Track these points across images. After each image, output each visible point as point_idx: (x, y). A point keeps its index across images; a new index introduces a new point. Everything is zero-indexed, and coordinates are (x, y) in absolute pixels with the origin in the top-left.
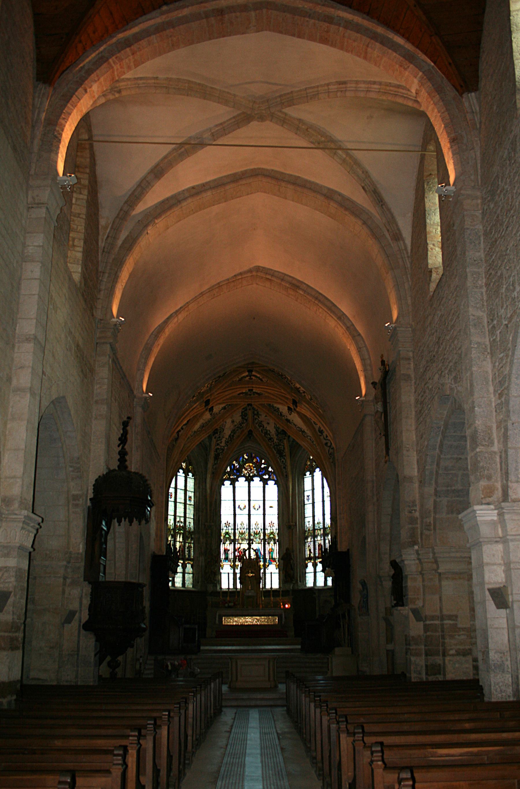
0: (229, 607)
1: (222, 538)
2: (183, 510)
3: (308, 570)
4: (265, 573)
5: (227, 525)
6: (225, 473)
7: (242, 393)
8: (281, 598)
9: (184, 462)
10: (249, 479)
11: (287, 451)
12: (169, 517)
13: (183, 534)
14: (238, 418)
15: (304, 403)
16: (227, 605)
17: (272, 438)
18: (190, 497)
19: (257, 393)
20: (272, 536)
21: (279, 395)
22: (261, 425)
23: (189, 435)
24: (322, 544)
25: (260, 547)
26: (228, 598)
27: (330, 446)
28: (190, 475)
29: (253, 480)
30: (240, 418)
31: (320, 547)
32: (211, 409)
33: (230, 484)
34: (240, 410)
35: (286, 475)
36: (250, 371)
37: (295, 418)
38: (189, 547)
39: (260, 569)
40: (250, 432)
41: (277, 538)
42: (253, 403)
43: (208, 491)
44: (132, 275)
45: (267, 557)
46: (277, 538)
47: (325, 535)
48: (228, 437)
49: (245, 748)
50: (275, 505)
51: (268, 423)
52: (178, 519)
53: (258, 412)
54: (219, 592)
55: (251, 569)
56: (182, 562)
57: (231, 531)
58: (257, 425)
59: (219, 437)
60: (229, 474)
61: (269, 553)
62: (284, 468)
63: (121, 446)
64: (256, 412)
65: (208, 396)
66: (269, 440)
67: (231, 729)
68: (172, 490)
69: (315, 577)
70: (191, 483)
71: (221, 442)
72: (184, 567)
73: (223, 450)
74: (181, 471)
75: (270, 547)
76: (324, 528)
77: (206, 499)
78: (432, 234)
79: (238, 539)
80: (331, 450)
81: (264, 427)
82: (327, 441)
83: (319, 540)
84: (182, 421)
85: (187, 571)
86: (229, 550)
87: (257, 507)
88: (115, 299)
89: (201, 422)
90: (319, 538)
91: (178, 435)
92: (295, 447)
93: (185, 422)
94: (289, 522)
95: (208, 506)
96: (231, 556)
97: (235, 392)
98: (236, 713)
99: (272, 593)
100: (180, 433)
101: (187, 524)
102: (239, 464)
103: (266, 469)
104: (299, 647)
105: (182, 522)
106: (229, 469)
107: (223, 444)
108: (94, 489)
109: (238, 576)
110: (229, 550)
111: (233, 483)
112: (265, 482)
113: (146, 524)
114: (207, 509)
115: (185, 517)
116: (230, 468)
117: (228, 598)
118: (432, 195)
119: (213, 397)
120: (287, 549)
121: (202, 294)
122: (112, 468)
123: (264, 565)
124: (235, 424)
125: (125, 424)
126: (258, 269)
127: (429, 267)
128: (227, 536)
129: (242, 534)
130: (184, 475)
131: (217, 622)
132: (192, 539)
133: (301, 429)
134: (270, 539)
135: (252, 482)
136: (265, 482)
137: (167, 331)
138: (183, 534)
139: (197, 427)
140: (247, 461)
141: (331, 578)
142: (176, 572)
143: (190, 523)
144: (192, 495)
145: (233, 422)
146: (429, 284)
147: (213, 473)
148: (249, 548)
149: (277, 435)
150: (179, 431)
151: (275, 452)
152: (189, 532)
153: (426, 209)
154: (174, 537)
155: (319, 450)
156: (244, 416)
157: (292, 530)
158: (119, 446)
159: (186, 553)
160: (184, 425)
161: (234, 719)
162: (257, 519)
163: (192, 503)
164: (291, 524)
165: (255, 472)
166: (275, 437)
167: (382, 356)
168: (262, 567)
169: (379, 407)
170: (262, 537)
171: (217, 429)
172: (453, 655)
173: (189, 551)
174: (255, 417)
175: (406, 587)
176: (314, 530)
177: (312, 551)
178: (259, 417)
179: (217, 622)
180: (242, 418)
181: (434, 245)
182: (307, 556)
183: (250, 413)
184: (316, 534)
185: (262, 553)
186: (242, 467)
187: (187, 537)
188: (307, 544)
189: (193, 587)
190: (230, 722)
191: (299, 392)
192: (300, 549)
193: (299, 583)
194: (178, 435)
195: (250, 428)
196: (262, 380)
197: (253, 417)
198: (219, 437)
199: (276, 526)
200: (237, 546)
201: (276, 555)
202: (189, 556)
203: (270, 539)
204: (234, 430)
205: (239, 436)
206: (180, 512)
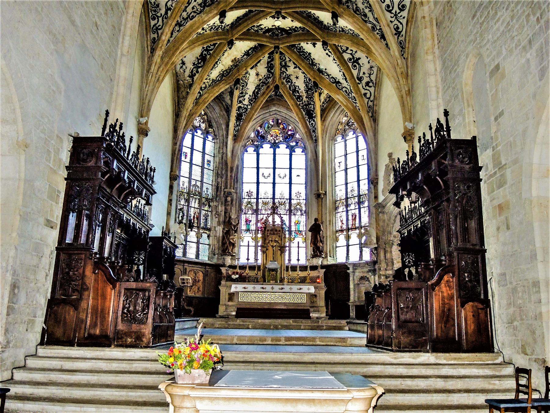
2: (199, 174)
5: (249, 194)
10: (275, 146)
14: (262, 69)
17: (301, 96)
22: (288, 78)
27: (369, 98)
28: (210, 138)
29: (279, 147)
31: (354, 216)
33: (254, 151)
35: (316, 140)
38: (206, 216)
41: (304, 209)
43: (229, 154)
45: (293, 228)
46: (304, 209)
48: (251, 94)
50: (303, 173)
51: (297, 78)
52: (193, 183)
53: (286, 63)
58: (284, 81)
62: (314, 131)
64: (283, 63)
66: (297, 99)
70: (210, 146)
73: (246, 109)
75: (297, 219)
76: (359, 196)
79: (261, 210)
81: (292, 82)
82: (366, 91)
85: (201, 241)
86: (250, 221)
87: (282, 176)
90: (352, 207)
94: (318, 190)
96: (253, 227)
101: (204, 189)
107: (246, 102)
110: (250, 221)
112: (292, 150)
114: (227, 175)
115: (202, 181)
124: (261, 78)
134: (296, 209)
135: (277, 149)
136: (292, 150)
138: (199, 199)
145: (257, 74)
147: (235, 136)
149: (307, 92)
151: (304, 113)
152: (207, 199)
157: (322, 199)
162: (282, 190)
164: (321, 192)
165: (281, 139)
166: (305, 95)
170: (287, 207)
174: (282, 69)
176: (347, 198)
177: (345, 222)
178: (287, 70)
179: (96, 248)
180: (268, 71)
184: (349, 202)
185: (288, 225)
187: (204, 204)
192: (330, 221)
195: (277, 83)
197: (281, 70)
199: (303, 196)
201: (302, 227)
203: (296, 209)
204: (258, 86)
205: (264, 93)
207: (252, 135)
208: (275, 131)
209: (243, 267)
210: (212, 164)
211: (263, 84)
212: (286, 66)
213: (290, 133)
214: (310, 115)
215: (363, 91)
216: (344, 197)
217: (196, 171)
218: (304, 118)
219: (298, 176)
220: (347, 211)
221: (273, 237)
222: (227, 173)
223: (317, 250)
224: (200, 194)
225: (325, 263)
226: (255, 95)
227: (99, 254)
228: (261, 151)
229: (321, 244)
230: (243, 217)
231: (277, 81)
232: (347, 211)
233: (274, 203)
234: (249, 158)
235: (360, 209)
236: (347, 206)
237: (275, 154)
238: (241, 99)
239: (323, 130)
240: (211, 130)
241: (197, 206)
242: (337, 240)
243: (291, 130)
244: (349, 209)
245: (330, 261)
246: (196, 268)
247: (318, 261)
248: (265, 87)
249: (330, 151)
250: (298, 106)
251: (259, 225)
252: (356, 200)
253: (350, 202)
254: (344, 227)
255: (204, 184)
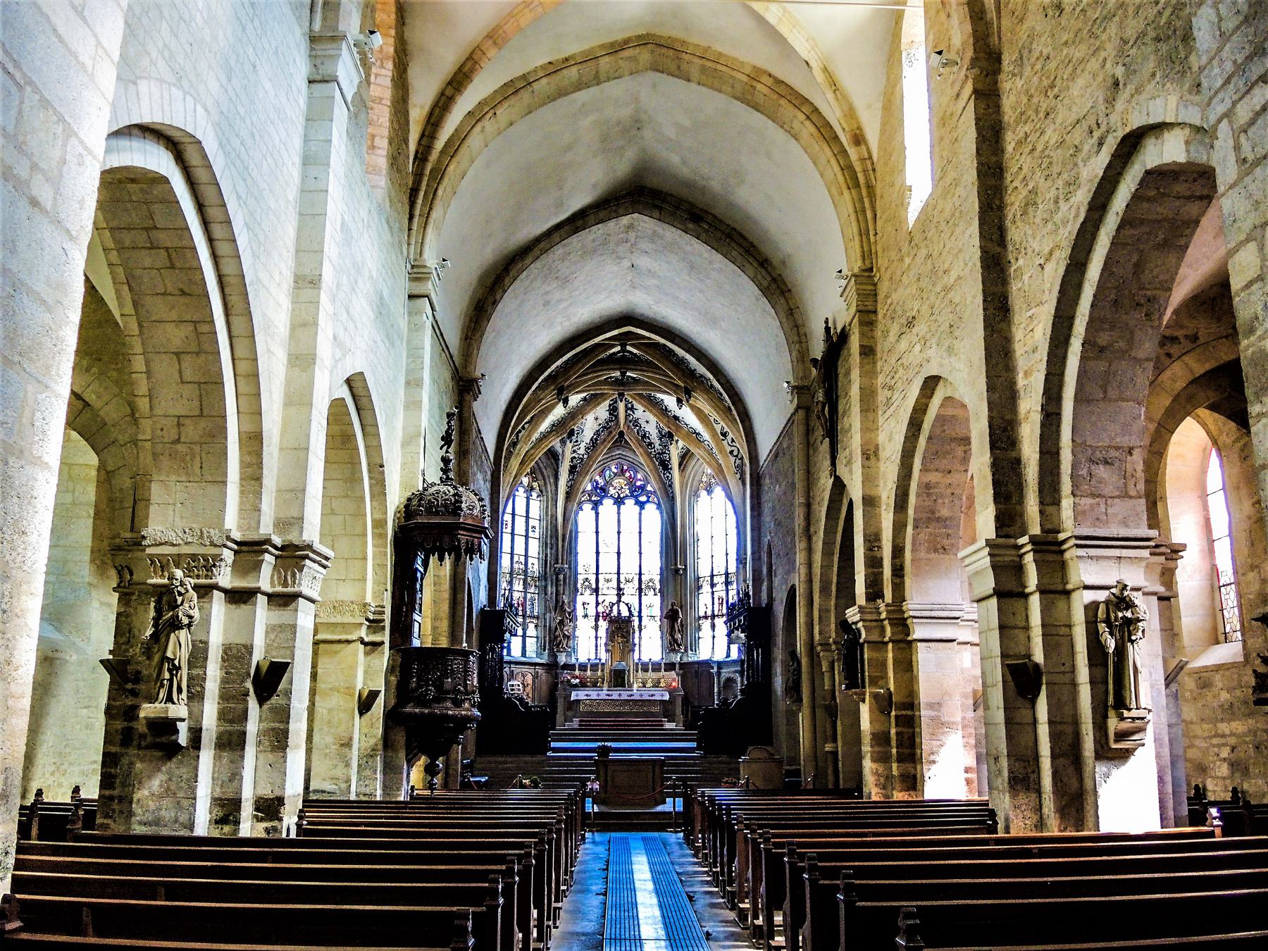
10: (619, 501)
22: (636, 423)
28: (534, 495)
41: (658, 587)
70: (535, 507)
76: (727, 574)
107: (582, 451)
134: (648, 587)
136: (641, 505)
166: (657, 443)
176: (712, 576)
207: (589, 488)
208: (619, 482)
209: (583, 667)
210: (537, 530)
213: (639, 483)
214: (665, 465)
215: (729, 448)
217: (519, 542)
218: (657, 470)
221: (621, 630)
222: (560, 544)
223: (672, 644)
225: (685, 660)
226: (594, 442)
227: (784, 933)
228: (601, 508)
230: (580, 599)
233: (619, 581)
234: (585, 517)
235: (727, 591)
236: (713, 585)
239: (682, 483)
240: (535, 485)
242: (699, 629)
245: (691, 658)
246: (525, 669)
247: (676, 658)
248: (606, 432)
249: (692, 509)
253: (716, 580)
254: (709, 613)
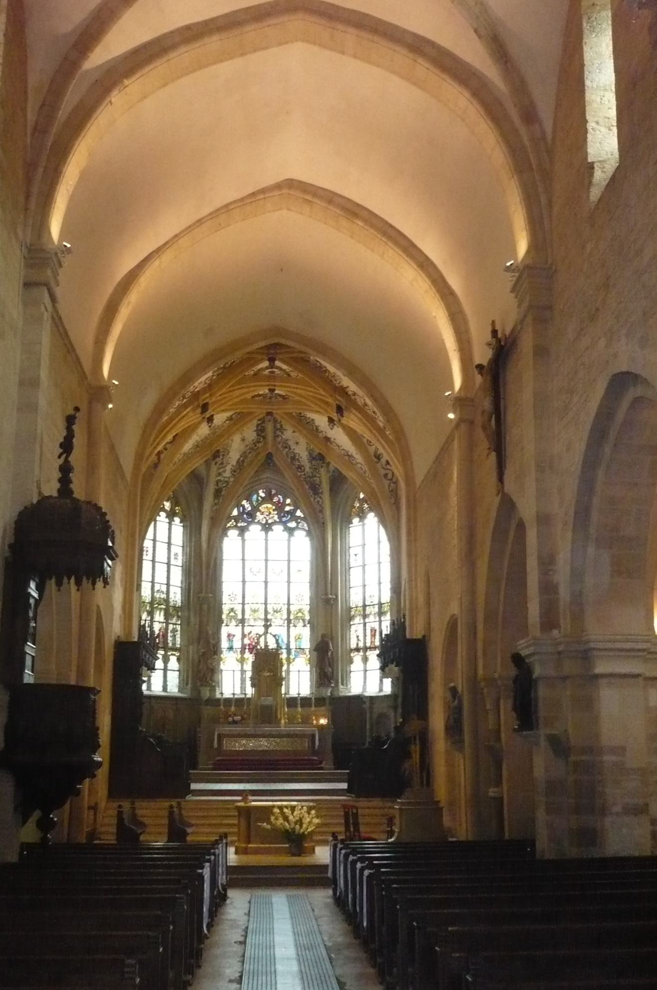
0: (235, 722)
1: (224, 617)
3: (353, 667)
4: (288, 671)
6: (230, 518)
7: (259, 395)
8: (313, 708)
9: (167, 501)
11: (325, 487)
12: (144, 584)
13: (165, 609)
14: (250, 433)
15: (354, 411)
16: (230, 719)
18: (176, 554)
19: (280, 395)
20: (300, 615)
21: (314, 397)
22: (286, 446)
23: (176, 459)
24: (377, 628)
25: (282, 632)
26: (233, 709)
27: (391, 479)
30: (255, 433)
32: (210, 420)
34: (255, 422)
36: (272, 360)
37: (339, 436)
38: (174, 631)
39: (282, 665)
40: (269, 456)
41: (307, 617)
42: (274, 412)
44: (84, 176)
45: (293, 646)
47: (381, 613)
48: (235, 463)
49: (273, 982)
52: (157, 587)
53: (281, 426)
54: (219, 700)
55: (268, 665)
56: (163, 652)
57: (238, 608)
59: (222, 463)
60: (237, 519)
61: (296, 640)
62: (321, 511)
63: (64, 456)
65: (206, 398)
67: (246, 937)
68: (148, 544)
69: (367, 679)
71: (224, 472)
72: (166, 660)
74: (163, 514)
76: (380, 605)
77: (201, 557)
78: (595, 105)
80: (392, 485)
82: (387, 472)
83: (372, 622)
84: (165, 436)
88: (56, 210)
89: (195, 439)
90: (371, 618)
91: (159, 459)
92: (337, 481)
93: (170, 437)
94: (326, 594)
95: (203, 573)
96: (237, 644)
97: (248, 392)
98: (250, 902)
99: (299, 702)
100: (162, 456)
102: (251, 504)
103: (292, 513)
104: (344, 786)
105: (163, 592)
106: (235, 513)
107: (227, 474)
108: (15, 529)
109: (249, 674)
111: (242, 531)
113: (105, 587)
114: (201, 573)
115: (168, 585)
116: (239, 510)
117: (233, 709)
118: (595, 40)
119: (214, 399)
120: (323, 636)
121: (200, 222)
122: (46, 494)
123: (288, 659)
124: (247, 442)
125: (70, 420)
126: (291, 184)
127: (590, 160)
128: (232, 614)
129: (255, 611)
130: (167, 520)
131: (216, 745)
132: (178, 617)
133: (347, 452)
137: (144, 281)
138: (165, 609)
139: (188, 446)
140: (264, 500)
141: (390, 680)
142: (152, 668)
143: (176, 596)
144: (179, 551)
145: (243, 440)
146: (589, 188)
148: (266, 633)
149: (310, 462)
150: (159, 453)
151: (307, 487)
152: (174, 607)
153: (585, 63)
154: (151, 613)
155: (374, 486)
156: (261, 430)
158: (59, 457)
159: (170, 639)
160: (168, 443)
161: (249, 914)
163: (180, 563)
165: (276, 518)
167: (493, 323)
168: (284, 662)
169: (487, 404)
170: (285, 616)
171: (218, 451)
172: (617, 814)
173: (174, 636)
175: (536, 699)
176: (365, 606)
177: (361, 638)
179: (216, 745)
180: (258, 435)
181: (597, 123)
182: (353, 646)
183: (269, 427)
184: (367, 612)
186: (255, 509)
188: (353, 628)
189: (179, 691)
190: (242, 921)
191: (347, 393)
193: (341, 687)
194: (159, 459)
196: (289, 375)
198: (222, 463)
200: (247, 630)
201: (306, 644)
202: (174, 644)
203: (296, 618)
204: (244, 453)
206: (161, 577)
211: (253, 448)
212: (282, 429)
216: (361, 604)
217: (161, 570)
219: (299, 571)
220: (365, 624)
224: (167, 601)
226: (240, 464)
229: (330, 670)
231: (270, 446)
232: (365, 624)
237: (266, 540)
238: (221, 470)
241: (162, 619)
243: (289, 505)
244: (367, 620)
248: (254, 453)
250: (298, 477)
251: (247, 641)
252: (376, 609)
255: (171, 588)
